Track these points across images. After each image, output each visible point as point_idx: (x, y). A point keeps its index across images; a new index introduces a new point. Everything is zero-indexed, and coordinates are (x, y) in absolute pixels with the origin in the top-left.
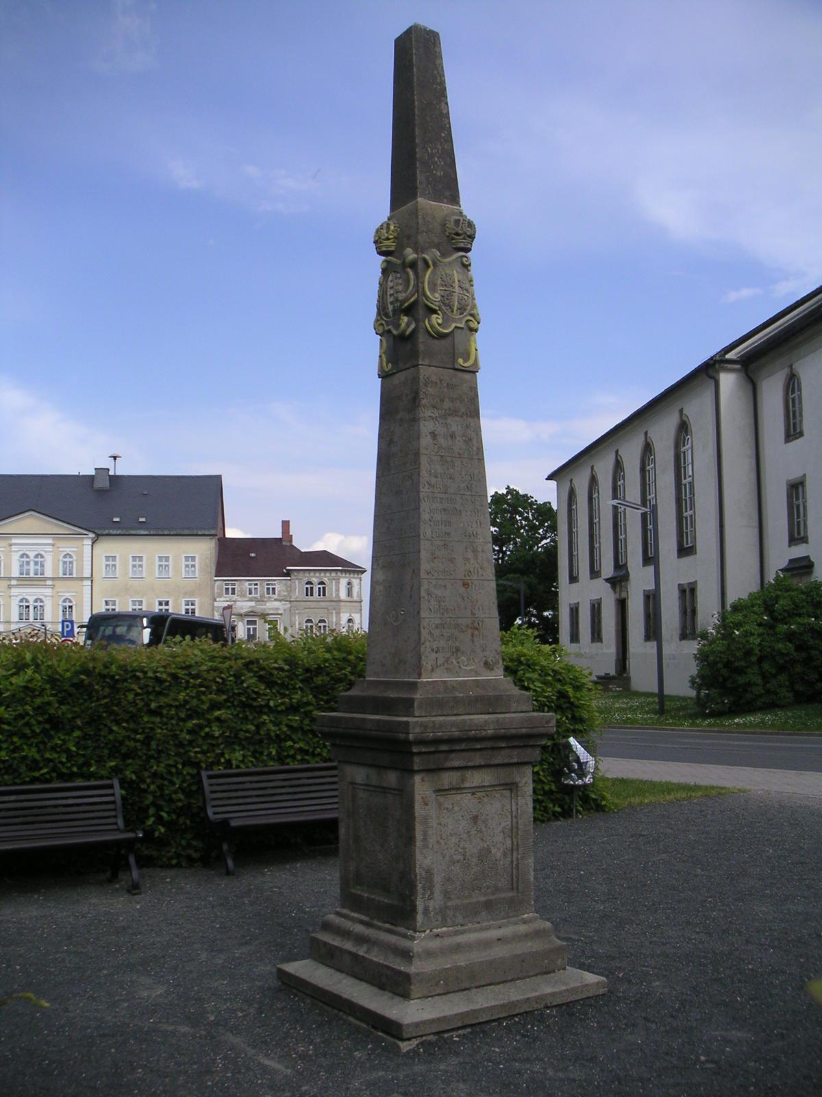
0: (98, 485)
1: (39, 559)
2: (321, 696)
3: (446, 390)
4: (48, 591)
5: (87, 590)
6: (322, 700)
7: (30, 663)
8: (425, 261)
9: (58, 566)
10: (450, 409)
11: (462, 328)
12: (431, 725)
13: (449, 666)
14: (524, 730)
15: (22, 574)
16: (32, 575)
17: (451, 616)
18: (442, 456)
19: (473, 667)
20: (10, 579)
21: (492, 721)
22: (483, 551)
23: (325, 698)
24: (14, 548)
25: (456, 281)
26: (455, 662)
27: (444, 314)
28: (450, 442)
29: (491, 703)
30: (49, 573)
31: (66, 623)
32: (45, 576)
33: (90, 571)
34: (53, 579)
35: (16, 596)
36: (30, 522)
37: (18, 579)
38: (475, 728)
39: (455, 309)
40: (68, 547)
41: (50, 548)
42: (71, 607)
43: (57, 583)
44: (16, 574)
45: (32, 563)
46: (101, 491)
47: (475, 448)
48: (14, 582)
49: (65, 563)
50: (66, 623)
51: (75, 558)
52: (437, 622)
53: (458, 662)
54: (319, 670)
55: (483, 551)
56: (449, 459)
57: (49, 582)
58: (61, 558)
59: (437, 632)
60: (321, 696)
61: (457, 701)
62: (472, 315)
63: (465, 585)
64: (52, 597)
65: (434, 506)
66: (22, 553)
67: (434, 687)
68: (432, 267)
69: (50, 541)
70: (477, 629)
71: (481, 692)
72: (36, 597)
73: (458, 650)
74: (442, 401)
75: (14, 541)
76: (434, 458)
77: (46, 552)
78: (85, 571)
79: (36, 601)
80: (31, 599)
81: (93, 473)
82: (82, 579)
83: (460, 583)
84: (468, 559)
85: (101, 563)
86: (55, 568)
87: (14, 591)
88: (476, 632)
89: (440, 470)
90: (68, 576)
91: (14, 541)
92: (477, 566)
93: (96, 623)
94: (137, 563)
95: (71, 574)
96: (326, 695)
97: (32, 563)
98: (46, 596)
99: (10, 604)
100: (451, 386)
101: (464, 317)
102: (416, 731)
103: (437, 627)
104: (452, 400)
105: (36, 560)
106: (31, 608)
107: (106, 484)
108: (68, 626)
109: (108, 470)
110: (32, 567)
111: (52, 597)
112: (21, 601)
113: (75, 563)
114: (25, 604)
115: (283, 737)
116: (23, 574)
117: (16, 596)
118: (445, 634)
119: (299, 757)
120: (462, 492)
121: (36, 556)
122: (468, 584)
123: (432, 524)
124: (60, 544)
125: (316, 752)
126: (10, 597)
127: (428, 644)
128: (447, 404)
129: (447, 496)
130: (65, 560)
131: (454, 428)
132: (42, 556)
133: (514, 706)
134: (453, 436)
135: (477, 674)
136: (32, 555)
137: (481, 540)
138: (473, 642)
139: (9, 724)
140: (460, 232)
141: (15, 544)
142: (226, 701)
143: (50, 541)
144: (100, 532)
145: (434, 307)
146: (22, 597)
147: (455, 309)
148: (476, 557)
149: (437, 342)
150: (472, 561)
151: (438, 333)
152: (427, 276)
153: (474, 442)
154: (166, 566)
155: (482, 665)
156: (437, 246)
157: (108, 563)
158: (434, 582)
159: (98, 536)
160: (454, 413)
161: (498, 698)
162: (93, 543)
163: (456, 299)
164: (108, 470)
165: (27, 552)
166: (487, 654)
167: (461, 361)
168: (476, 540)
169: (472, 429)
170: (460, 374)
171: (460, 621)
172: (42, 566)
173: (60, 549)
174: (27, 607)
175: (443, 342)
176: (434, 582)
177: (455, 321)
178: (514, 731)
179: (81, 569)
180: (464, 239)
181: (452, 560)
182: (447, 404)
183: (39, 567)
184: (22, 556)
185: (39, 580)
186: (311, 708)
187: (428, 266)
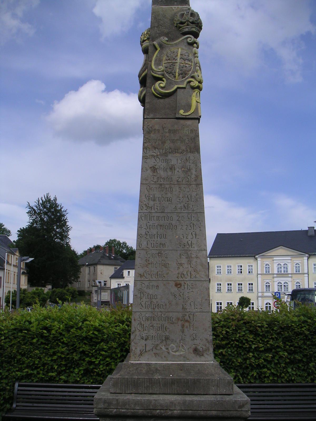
0: (310, 234)
1: (285, 266)
2: (287, 343)
3: (167, 134)
4: (290, 279)
5: (306, 279)
6: (288, 345)
7: (125, 320)
8: (154, 46)
9: (294, 268)
10: (170, 148)
11: (184, 88)
12: (114, 402)
13: (157, 352)
14: (214, 413)
15: (278, 272)
16: (283, 272)
17: (162, 310)
18: (161, 185)
19: (182, 353)
20: (273, 274)
21: (179, 403)
22: (197, 257)
23: (289, 344)
24: (275, 261)
25: (179, 55)
26: (163, 348)
27: (167, 79)
28: (170, 173)
29: (189, 384)
30: (289, 271)
31: (276, 294)
32: (288, 273)
33: (307, 269)
34: (291, 274)
35: (276, 281)
36: (281, 251)
37: (277, 274)
38: (160, 408)
39: (177, 74)
40: (297, 260)
41: (290, 261)
42: (269, 286)
43: (293, 275)
44: (276, 272)
45: (282, 268)
46: (311, 237)
47: (193, 176)
48: (275, 276)
49: (296, 267)
50: (276, 294)
51: (270, 266)
52: (147, 315)
53: (167, 349)
54: (288, 328)
55: (197, 257)
56: (167, 186)
57: (290, 275)
58: (294, 265)
59: (147, 324)
60: (287, 343)
61: (152, 382)
62: (193, 77)
63: (178, 285)
64: (291, 281)
65: (151, 223)
66: (278, 263)
67: (137, 369)
68: (159, 49)
69: (290, 258)
70: (187, 321)
71: (183, 375)
72: (285, 282)
73: (167, 338)
74: (164, 143)
75: (274, 259)
76: (152, 186)
77: (288, 263)
78: (305, 270)
79: (285, 283)
80: (283, 282)
81: (307, 229)
82: (304, 274)
83: (173, 284)
84: (181, 264)
85: (312, 267)
86: (262, 270)
87: (276, 279)
88: (187, 324)
89: (158, 195)
90: (298, 272)
91: (274, 259)
92: (190, 269)
93: (295, 294)
94: (219, 268)
95: (299, 272)
96: (290, 342)
97: (282, 268)
98: (289, 281)
99: (274, 285)
100: (174, 132)
101: (186, 79)
102: (100, 407)
103: (147, 319)
104: (173, 141)
105: (284, 266)
106: (283, 286)
107: (313, 233)
108: (277, 295)
109: (314, 227)
110: (282, 269)
111: (291, 281)
112: (279, 283)
113: (300, 267)
114: (280, 284)
115: (262, 366)
116: (279, 272)
117: (276, 281)
118: (155, 325)
119: (271, 378)
120: (179, 211)
121: (284, 265)
122: (180, 284)
123: (148, 237)
124: (293, 259)
125: (282, 376)
126: (274, 282)
127: (137, 333)
128: (168, 145)
129: (164, 215)
130: (296, 266)
131: (174, 162)
132: (287, 265)
133: (213, 389)
134: (172, 168)
135: (185, 358)
136: (282, 264)
137: (196, 249)
138: (183, 332)
139: (106, 351)
140: (183, 21)
141: (275, 260)
142: (227, 344)
143: (290, 258)
144: (310, 254)
145: (157, 76)
146: (279, 282)
147: (177, 74)
148: (190, 262)
149: (162, 101)
150: (186, 266)
151: (160, 94)
152: (155, 55)
153: (193, 172)
154: (230, 269)
155: (192, 352)
156: (166, 35)
157: (218, 269)
158: (147, 283)
159: (310, 255)
160: (175, 151)
161: (196, 382)
162: (308, 259)
163: (178, 67)
164: (314, 227)
165: (280, 263)
166: (196, 342)
167: (182, 112)
168: (191, 249)
169: (191, 161)
170: (182, 121)
171: (171, 315)
172: (287, 269)
173: (264, 262)
174: (281, 286)
175: (167, 100)
176: (147, 283)
177: (176, 83)
178: (202, 413)
179: (303, 270)
180: (188, 25)
181: (165, 266)
182: (168, 145)
183: (285, 269)
184: (278, 265)
185: (285, 274)
186: (279, 350)
187: (156, 49)
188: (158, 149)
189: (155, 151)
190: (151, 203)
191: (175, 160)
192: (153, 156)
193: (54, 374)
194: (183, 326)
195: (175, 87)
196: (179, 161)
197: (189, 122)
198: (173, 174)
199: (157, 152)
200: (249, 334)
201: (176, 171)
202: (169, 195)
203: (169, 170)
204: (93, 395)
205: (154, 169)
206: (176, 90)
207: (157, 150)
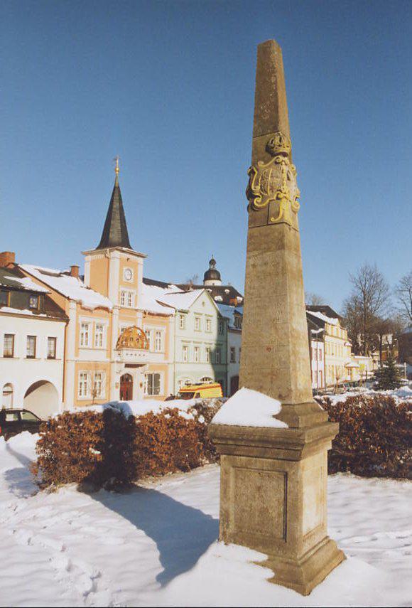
27: (263, 195)
55: (282, 328)
83: (265, 348)
88: (274, 377)
100: (267, 235)
153: (281, 264)
160: (269, 249)
190: (252, 291)
191: (269, 256)
193: (86, 529)
194: (272, 378)
195: (268, 201)
197: (277, 226)
199: (256, 253)
202: (264, 284)
205: (254, 266)
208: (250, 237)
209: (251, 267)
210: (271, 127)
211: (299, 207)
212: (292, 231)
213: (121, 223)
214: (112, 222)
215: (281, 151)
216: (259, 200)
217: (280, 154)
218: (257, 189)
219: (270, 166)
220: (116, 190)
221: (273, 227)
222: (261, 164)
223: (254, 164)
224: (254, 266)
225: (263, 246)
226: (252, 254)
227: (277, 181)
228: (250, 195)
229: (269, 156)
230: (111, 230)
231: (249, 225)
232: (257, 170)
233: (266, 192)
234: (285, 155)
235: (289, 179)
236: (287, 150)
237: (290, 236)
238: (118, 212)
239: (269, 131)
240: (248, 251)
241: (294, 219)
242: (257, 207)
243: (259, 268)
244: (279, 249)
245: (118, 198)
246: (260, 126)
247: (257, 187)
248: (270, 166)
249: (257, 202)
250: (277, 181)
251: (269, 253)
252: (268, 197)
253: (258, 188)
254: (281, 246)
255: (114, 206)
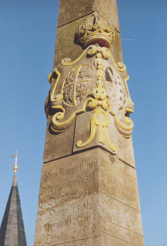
47: (91, 226)
100: (70, 172)
153: (91, 220)
160: (73, 195)
188: (54, 199)
189: (50, 203)
191: (72, 208)
192: (48, 209)
195: (73, 115)
196: (76, 209)
197: (88, 154)
198: (69, 228)
199: (53, 203)
200: (73, 235)
201: (72, 224)
203: (64, 224)
204: (102, 32)
206: (76, 118)
207: (53, 200)
208: (46, 177)
209: (43, 229)
210: (83, 8)
211: (132, 126)
212: (119, 165)
213: (18, 227)
214: (8, 227)
215: (95, 37)
216: (60, 115)
217: (94, 42)
218: (58, 99)
219: (78, 63)
220: (14, 190)
221: (80, 155)
222: (66, 62)
223: (57, 63)
224: (48, 227)
225: (64, 191)
226: (46, 206)
227: (87, 82)
228: (50, 110)
229: (80, 47)
230: (7, 236)
231: (45, 158)
232: (60, 70)
233: (72, 101)
234: (102, 43)
235: (108, 78)
236: (104, 36)
237: (112, 172)
238: (16, 215)
239: (80, 15)
240: (41, 201)
241: (121, 145)
242: (57, 128)
243: (57, 231)
244: (90, 193)
245: (15, 199)
246: (67, 10)
247: (57, 96)
248: (78, 63)
249: (57, 119)
250: (87, 82)
251: (74, 201)
252: (75, 109)
253: (60, 96)
254: (93, 187)
255: (11, 209)
